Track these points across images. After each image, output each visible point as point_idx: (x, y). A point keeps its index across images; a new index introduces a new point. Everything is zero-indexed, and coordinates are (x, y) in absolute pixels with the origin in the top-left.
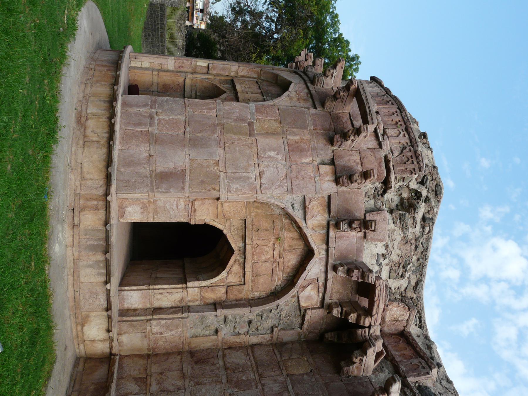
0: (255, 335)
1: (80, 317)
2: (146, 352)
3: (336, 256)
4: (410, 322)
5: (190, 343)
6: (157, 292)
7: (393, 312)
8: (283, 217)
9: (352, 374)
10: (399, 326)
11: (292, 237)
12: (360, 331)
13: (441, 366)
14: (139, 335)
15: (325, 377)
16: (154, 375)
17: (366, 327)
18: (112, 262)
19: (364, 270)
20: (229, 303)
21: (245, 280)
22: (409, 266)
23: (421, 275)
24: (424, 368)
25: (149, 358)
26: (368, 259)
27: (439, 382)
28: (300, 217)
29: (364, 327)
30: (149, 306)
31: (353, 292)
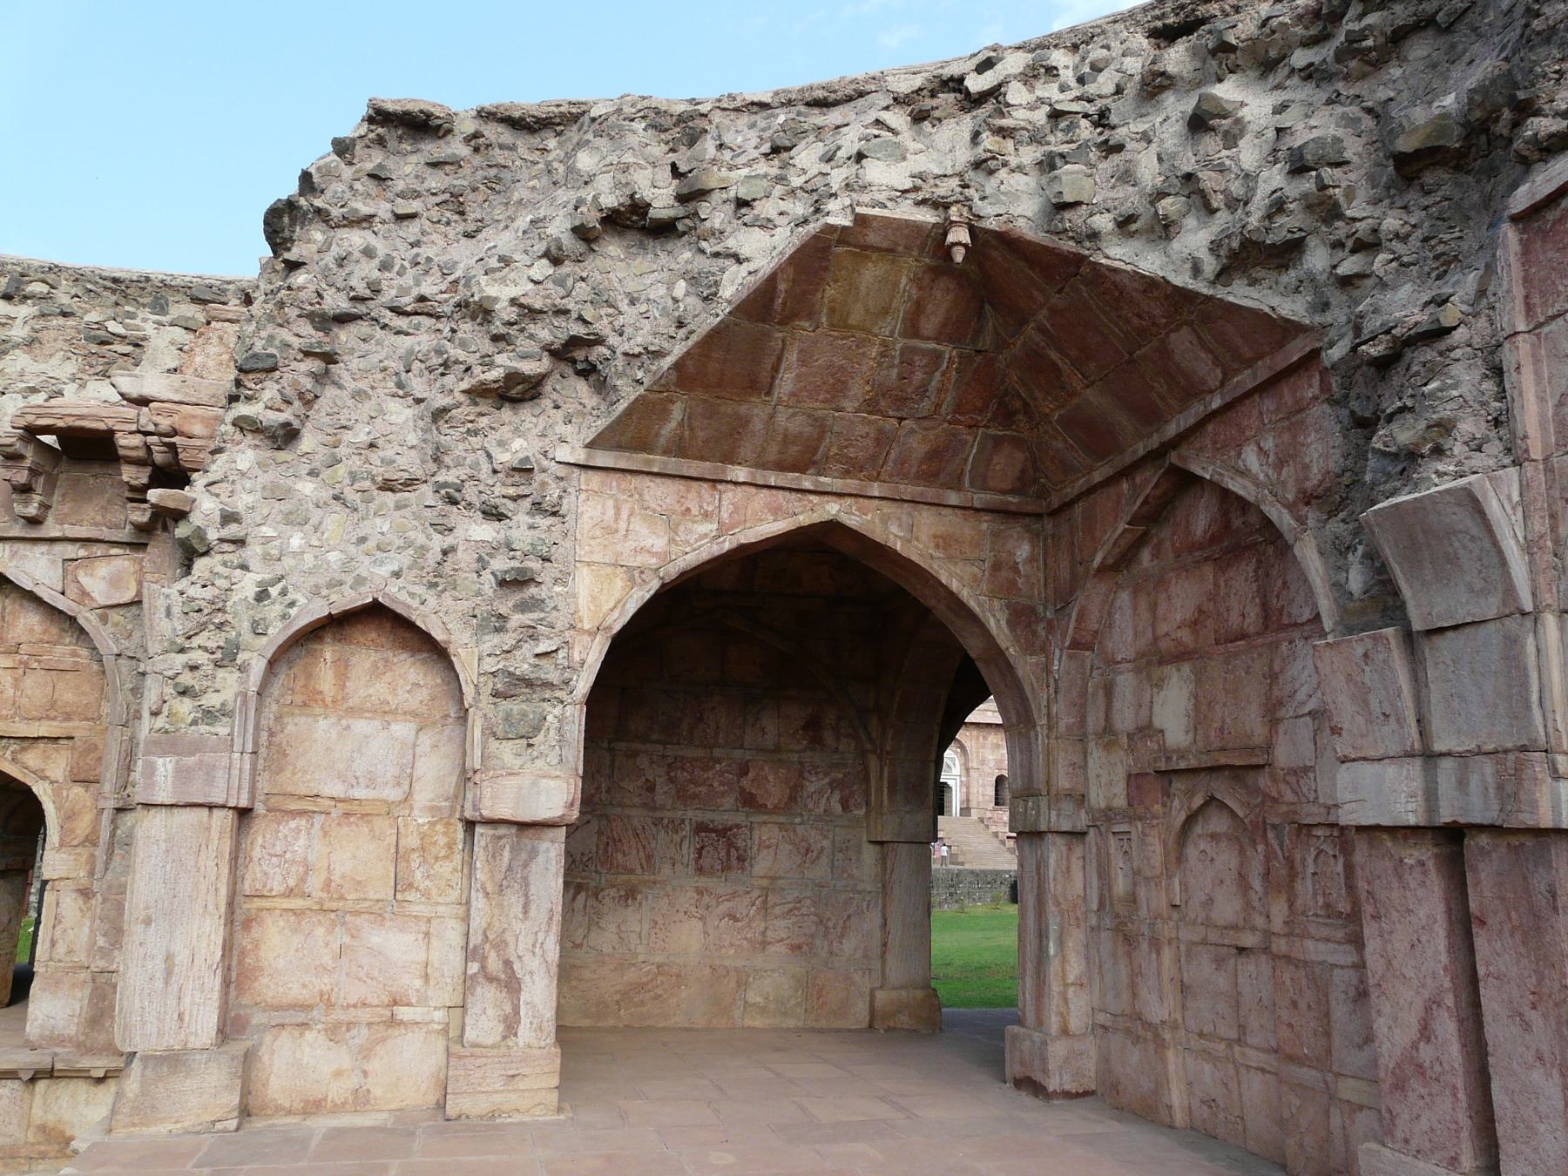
1: (42, 1148)
7: (211, 363)
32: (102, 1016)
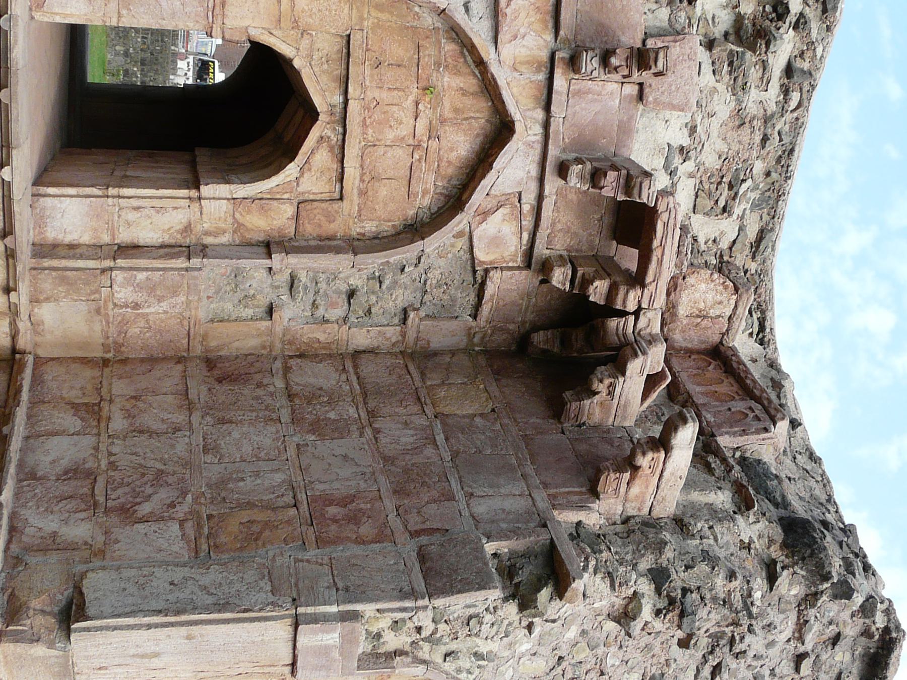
0: (362, 326)
2: (99, 354)
3: (567, 140)
4: (736, 323)
5: (205, 337)
6: (125, 205)
7: (697, 295)
8: (441, 37)
9: (589, 418)
10: (710, 332)
11: (461, 89)
12: (613, 323)
13: (800, 424)
14: (83, 307)
15: (526, 423)
16: (117, 400)
17: (629, 313)
18: (14, 112)
19: (631, 172)
20: (303, 243)
21: (342, 187)
22: (744, 186)
23: (774, 217)
24: (759, 420)
25: (107, 366)
26: (645, 154)
27: (790, 457)
28: (483, 36)
29: (623, 314)
30: (106, 239)
31: (604, 232)
32: (69, 284)
